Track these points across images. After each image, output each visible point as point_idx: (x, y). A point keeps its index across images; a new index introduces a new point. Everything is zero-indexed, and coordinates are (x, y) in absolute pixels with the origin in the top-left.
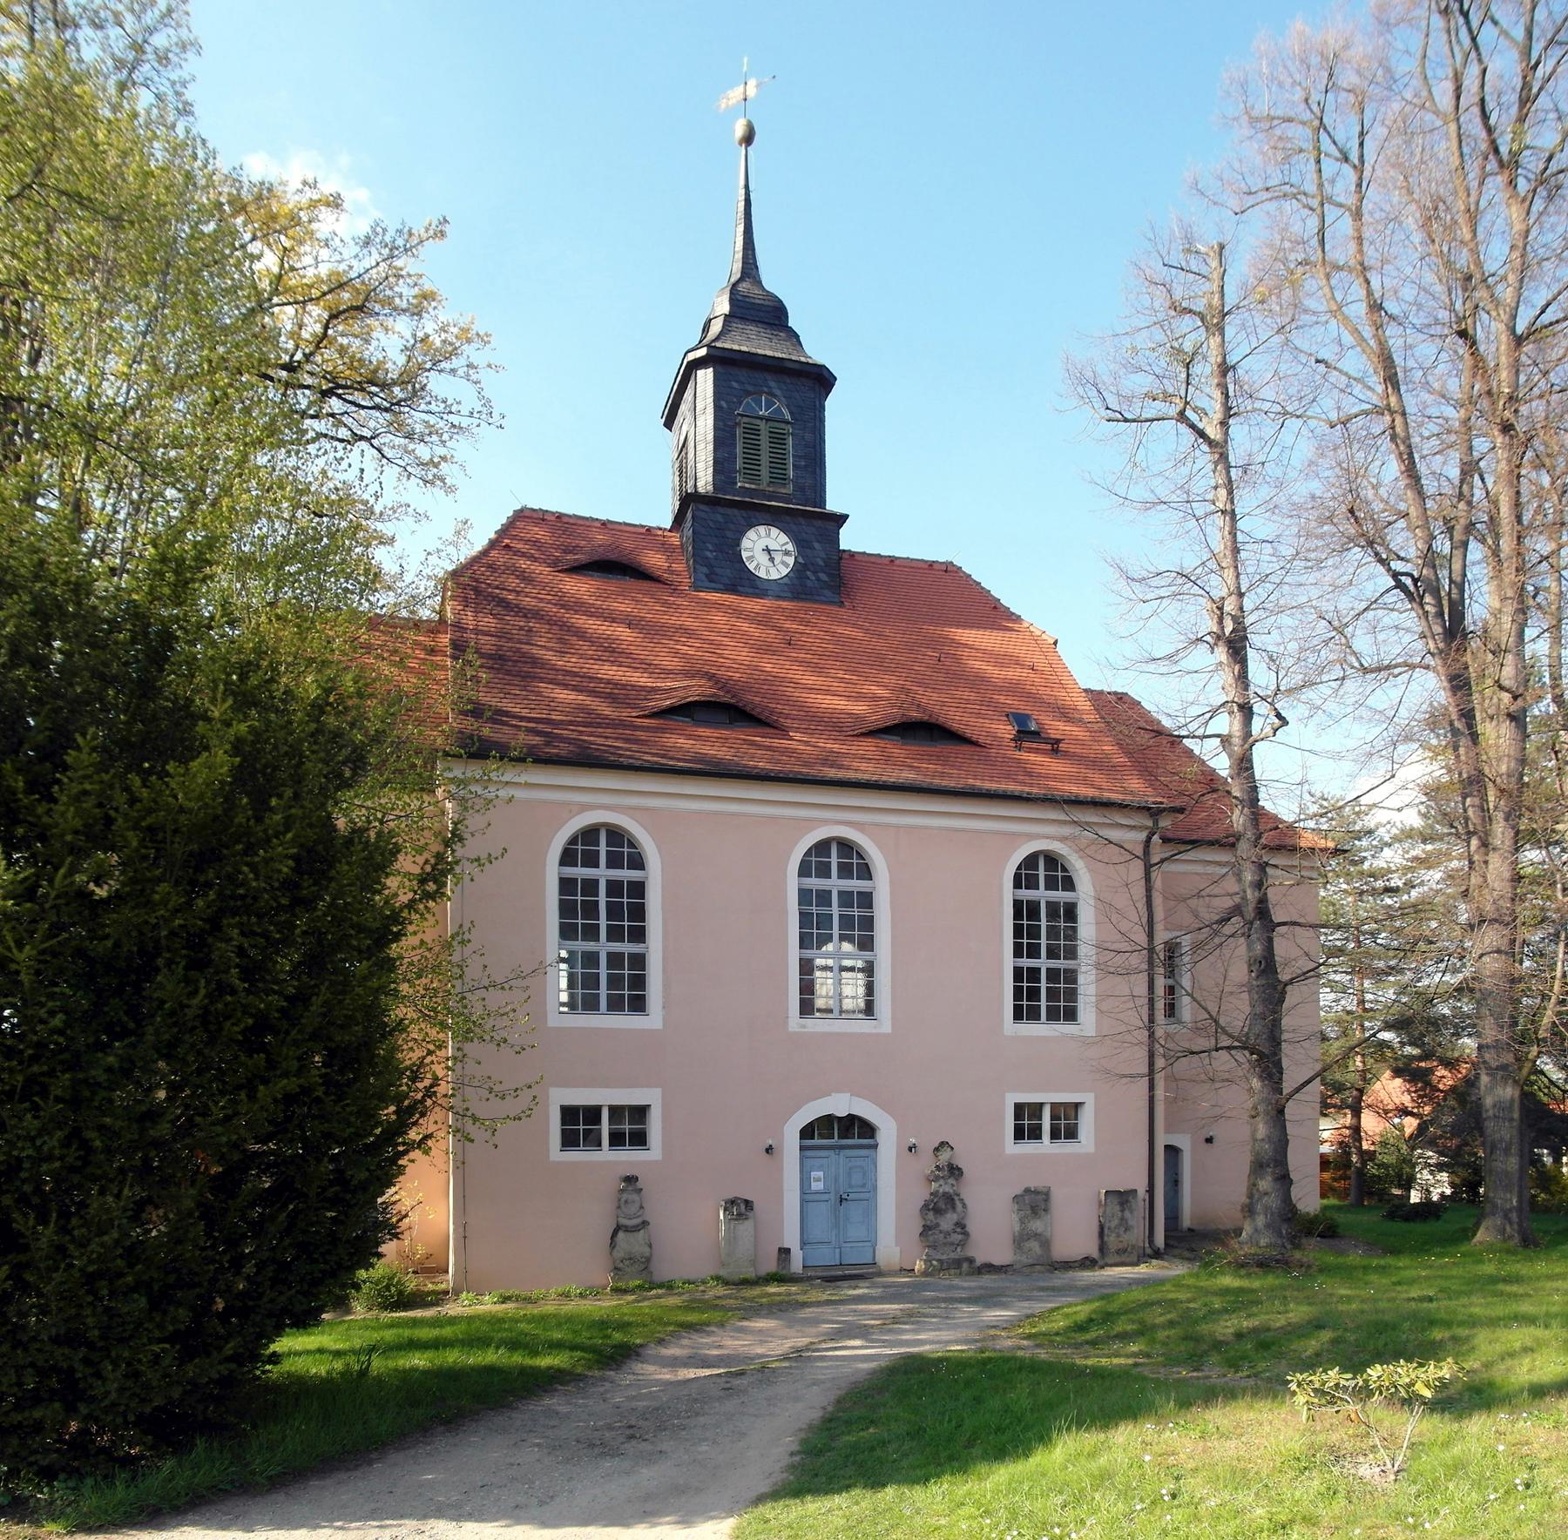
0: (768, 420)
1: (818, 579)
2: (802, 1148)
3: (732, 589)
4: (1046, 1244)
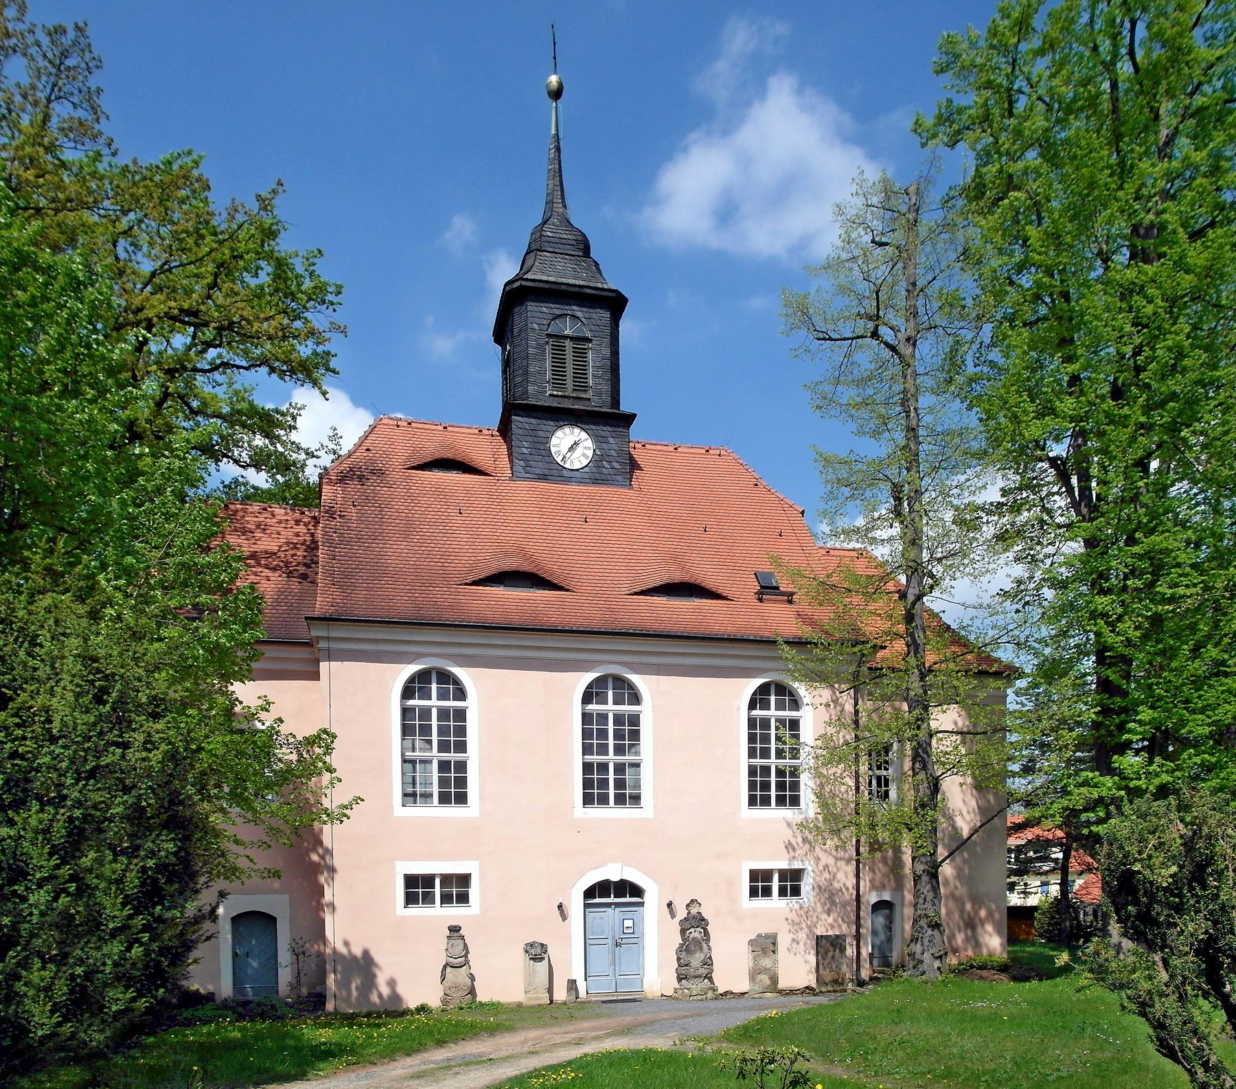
0: (572, 338)
1: (613, 468)
2: (586, 906)
3: (543, 478)
4: (774, 980)
